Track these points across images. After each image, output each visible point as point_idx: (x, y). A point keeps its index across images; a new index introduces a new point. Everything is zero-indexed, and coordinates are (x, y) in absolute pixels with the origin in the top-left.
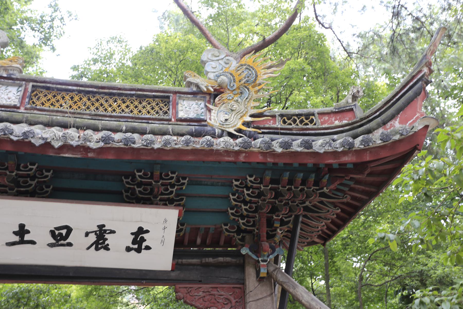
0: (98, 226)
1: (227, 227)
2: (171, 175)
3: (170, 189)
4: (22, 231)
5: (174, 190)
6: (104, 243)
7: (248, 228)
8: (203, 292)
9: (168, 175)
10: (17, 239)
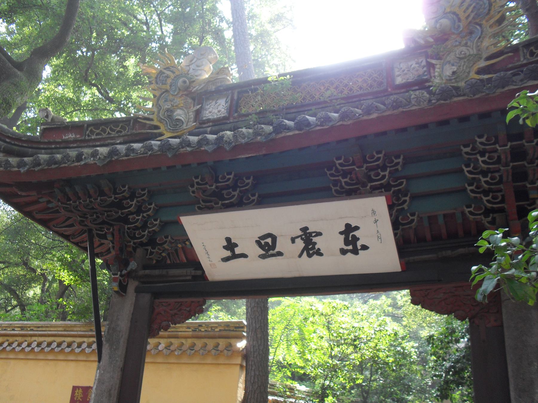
0: (301, 229)
1: (471, 209)
2: (377, 156)
3: (382, 173)
4: (230, 245)
5: (387, 173)
6: (313, 248)
7: (495, 206)
8: (444, 293)
9: (373, 156)
10: (228, 253)
